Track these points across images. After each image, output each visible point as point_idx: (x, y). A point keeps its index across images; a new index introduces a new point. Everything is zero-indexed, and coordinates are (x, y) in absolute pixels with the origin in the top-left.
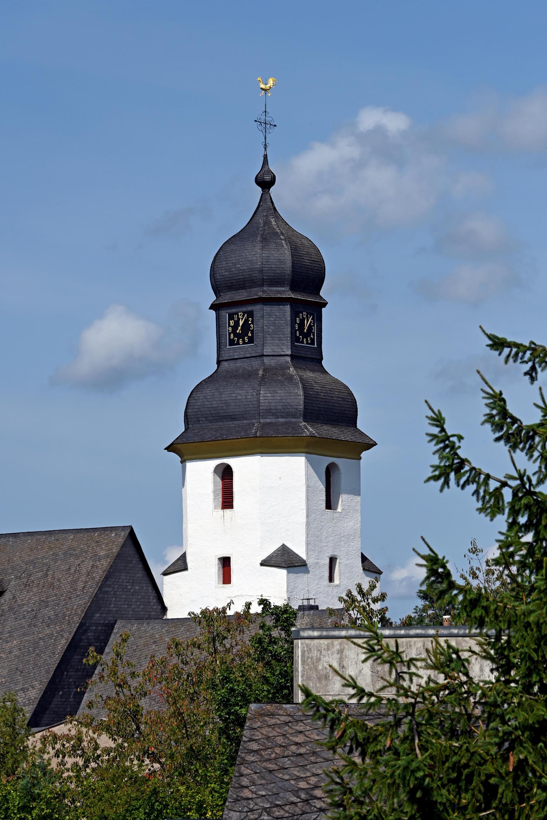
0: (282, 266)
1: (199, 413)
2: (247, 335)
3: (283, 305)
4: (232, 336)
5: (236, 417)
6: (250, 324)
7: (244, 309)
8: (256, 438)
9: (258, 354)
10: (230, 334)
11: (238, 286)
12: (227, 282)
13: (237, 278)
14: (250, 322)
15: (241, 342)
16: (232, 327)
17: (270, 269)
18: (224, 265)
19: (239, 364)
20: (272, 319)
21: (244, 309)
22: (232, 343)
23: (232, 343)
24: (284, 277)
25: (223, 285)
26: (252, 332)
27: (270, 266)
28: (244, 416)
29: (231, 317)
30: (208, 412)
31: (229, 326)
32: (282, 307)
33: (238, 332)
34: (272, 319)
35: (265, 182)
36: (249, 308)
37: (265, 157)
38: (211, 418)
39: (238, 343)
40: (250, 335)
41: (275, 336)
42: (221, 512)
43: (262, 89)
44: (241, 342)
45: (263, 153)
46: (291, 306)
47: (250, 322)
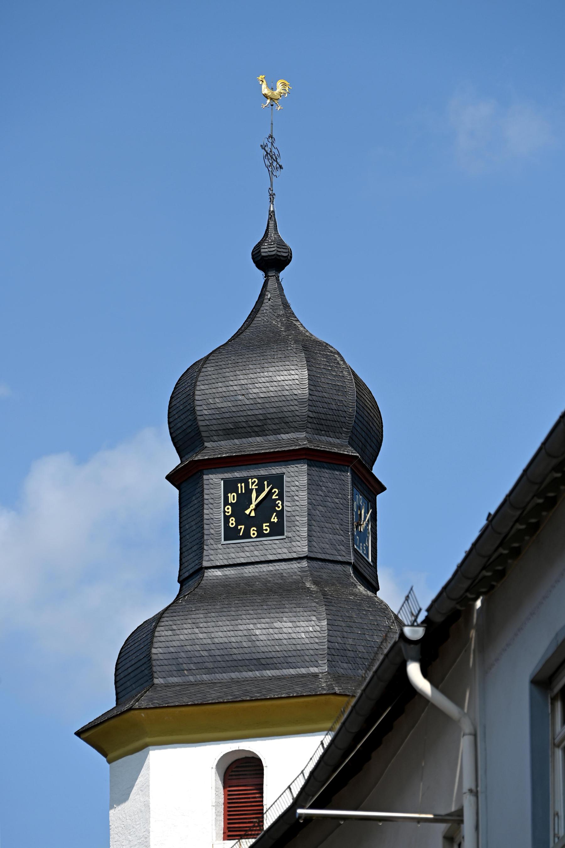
0: (341, 398)
1: (183, 655)
2: (268, 520)
3: (341, 471)
4: (232, 522)
5: (268, 661)
6: (276, 500)
7: (263, 472)
8: (332, 697)
9: (295, 555)
10: (227, 519)
11: (249, 429)
12: (226, 420)
13: (249, 413)
14: (274, 497)
15: (253, 531)
16: (231, 504)
17: (320, 399)
18: (220, 390)
19: (249, 571)
20: (320, 492)
21: (263, 472)
22: (231, 534)
23: (231, 534)
24: (343, 419)
25: (215, 428)
26: (280, 515)
27: (320, 394)
28: (289, 660)
29: (230, 486)
30: (205, 653)
31: (226, 503)
32: (337, 473)
33: (247, 512)
34: (320, 492)
35: (271, 261)
36: (275, 470)
37: (272, 214)
38: (210, 665)
39: (247, 535)
40: (274, 519)
41: (327, 525)
42: (222, 842)
43: (266, 96)
44: (253, 531)
45: (265, 207)
46: (353, 474)
47: (274, 497)
